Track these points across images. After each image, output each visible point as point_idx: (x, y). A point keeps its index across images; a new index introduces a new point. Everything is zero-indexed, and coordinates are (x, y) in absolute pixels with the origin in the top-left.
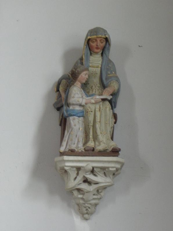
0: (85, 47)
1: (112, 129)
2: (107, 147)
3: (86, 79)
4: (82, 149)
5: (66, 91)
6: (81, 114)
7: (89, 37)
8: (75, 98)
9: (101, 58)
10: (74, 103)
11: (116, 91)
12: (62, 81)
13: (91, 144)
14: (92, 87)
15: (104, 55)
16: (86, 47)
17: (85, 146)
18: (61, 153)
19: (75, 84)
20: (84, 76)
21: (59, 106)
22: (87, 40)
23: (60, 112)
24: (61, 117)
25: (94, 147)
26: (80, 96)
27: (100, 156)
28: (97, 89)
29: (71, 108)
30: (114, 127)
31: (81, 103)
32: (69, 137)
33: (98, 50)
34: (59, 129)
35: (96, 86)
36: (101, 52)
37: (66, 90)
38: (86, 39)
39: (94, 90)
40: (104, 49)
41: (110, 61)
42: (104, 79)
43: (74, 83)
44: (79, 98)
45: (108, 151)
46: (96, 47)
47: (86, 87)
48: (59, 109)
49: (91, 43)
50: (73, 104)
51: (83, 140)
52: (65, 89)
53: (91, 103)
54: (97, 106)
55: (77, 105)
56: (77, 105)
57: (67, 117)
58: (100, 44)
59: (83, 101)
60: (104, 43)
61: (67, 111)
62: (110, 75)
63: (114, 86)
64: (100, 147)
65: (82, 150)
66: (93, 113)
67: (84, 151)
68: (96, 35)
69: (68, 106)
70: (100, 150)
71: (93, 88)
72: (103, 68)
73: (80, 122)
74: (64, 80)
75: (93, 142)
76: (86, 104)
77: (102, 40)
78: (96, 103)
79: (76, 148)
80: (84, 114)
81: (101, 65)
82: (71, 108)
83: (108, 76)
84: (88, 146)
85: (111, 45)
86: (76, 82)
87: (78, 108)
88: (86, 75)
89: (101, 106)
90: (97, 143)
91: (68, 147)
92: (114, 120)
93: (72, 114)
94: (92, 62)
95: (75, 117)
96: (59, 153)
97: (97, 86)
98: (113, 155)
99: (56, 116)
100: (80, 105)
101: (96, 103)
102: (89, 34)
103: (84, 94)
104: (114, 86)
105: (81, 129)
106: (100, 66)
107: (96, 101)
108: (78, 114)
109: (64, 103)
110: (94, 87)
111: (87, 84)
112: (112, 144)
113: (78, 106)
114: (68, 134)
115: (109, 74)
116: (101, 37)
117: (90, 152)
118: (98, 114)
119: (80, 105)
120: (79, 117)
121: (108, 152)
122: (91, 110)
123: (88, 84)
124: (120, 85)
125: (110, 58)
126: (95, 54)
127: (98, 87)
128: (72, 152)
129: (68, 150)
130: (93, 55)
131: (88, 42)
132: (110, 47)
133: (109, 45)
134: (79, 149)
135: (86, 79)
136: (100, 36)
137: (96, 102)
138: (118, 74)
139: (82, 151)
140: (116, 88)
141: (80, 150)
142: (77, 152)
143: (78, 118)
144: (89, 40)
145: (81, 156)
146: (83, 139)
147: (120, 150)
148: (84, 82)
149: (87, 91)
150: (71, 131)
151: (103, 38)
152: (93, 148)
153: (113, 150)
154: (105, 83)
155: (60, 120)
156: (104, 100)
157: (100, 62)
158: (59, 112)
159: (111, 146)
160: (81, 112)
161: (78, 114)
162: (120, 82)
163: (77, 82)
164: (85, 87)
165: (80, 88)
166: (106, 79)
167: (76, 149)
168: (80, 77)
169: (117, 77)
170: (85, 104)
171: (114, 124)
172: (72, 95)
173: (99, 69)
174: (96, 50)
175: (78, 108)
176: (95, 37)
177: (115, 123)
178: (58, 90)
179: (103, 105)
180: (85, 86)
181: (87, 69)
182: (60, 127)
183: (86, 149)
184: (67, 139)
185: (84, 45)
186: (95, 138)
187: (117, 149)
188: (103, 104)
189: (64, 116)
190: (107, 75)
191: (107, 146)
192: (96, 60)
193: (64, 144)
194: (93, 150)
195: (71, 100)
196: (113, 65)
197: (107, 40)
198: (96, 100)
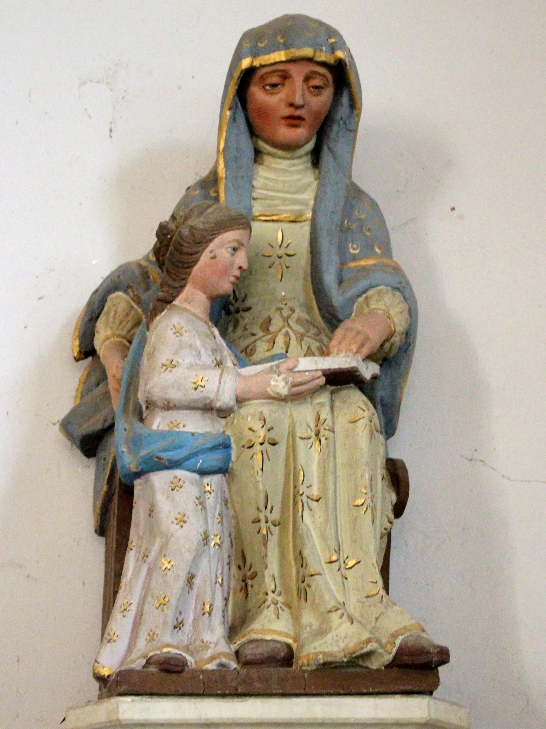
0: (228, 113)
1: (385, 539)
2: (369, 641)
3: (237, 273)
4: (226, 655)
5: (128, 349)
6: (213, 459)
7: (246, 63)
8: (177, 373)
9: (309, 178)
10: (175, 395)
11: (397, 339)
12: (108, 298)
13: (272, 626)
14: (266, 325)
15: (326, 158)
16: (234, 118)
17: (240, 641)
18: (101, 679)
19: (176, 302)
20: (224, 254)
21: (94, 425)
22: (236, 75)
23: (98, 462)
24: (105, 488)
25: (290, 641)
26: (207, 358)
27: (338, 694)
28: (296, 333)
29: (155, 427)
30: (389, 535)
31: (212, 396)
32: (147, 588)
33: (301, 132)
34: (94, 551)
35: (289, 317)
36: (310, 146)
37: (130, 342)
38: (230, 76)
39: (280, 340)
40: (323, 129)
41: (355, 194)
42: (329, 278)
43: (174, 297)
44: (204, 367)
45: (375, 664)
46: (288, 111)
47: (235, 326)
48: (91, 444)
49: (257, 93)
50: (169, 406)
51: (226, 605)
52: (119, 336)
53: (269, 397)
54: (304, 415)
55: (191, 407)
56: (191, 407)
57: (138, 475)
58: (308, 95)
59: (222, 385)
60: (328, 94)
61: (135, 442)
62: (362, 263)
63: (381, 311)
64: (337, 640)
65: (224, 660)
66: (282, 448)
67: (234, 665)
68: (286, 46)
69: (142, 420)
70: (329, 659)
71: (272, 329)
72: (321, 220)
73: (210, 500)
74: (120, 294)
75: (285, 614)
76: (240, 401)
77: (319, 74)
78: (297, 395)
79: (187, 649)
80: (228, 459)
81: (314, 211)
82: (159, 422)
83: (353, 264)
84: (254, 636)
85: (360, 109)
86: (183, 287)
87: (194, 425)
88: (235, 249)
89: (325, 414)
90: (308, 618)
91: (142, 644)
92: (393, 498)
93: (164, 455)
94: (264, 192)
95: (179, 473)
96: (96, 685)
97: (295, 315)
98: (409, 688)
99: (77, 484)
100: (208, 408)
101: (297, 395)
102: (247, 45)
103: (226, 351)
104: (381, 311)
105: (214, 541)
106: (309, 215)
107: (294, 385)
108: (194, 454)
109: (117, 403)
110: (277, 323)
111: (237, 311)
112: (391, 627)
113: (198, 415)
114: (144, 572)
115: (355, 258)
116: (310, 60)
117: (272, 670)
118: (310, 457)
119: (208, 408)
120: (203, 473)
121: (378, 670)
122: (272, 434)
123: (248, 309)
124: (412, 313)
125: (355, 179)
126: (279, 152)
127: (299, 321)
128: (163, 675)
129: (144, 662)
130: (268, 160)
131: (243, 84)
132: (358, 116)
133: (354, 105)
134: (209, 653)
135: (237, 273)
136: (308, 52)
137: (295, 390)
138: (401, 255)
139: (222, 665)
140: (400, 323)
141: (212, 658)
142: (193, 671)
143: (196, 476)
144: (250, 72)
145: (223, 696)
146: (226, 599)
147: (444, 656)
148: (225, 286)
149: (244, 344)
150: (162, 553)
151: (323, 64)
152: (289, 647)
153: (407, 659)
154: (337, 298)
155: (99, 503)
156: (338, 379)
157: (309, 196)
158: (92, 462)
159: (394, 636)
160: (214, 448)
161: (194, 454)
162: (412, 292)
163: (188, 288)
164: (231, 328)
165: (200, 319)
166: (340, 281)
167: (188, 658)
168: (204, 258)
169: (397, 270)
170: (232, 403)
171: (391, 515)
172: (163, 358)
173: (306, 228)
174: (284, 133)
175: (194, 425)
176: (280, 56)
177: (399, 509)
178: (87, 351)
179: (332, 408)
180: (228, 313)
181: (242, 221)
182: (102, 539)
183: (250, 652)
184: (135, 601)
185: (222, 107)
186: (301, 591)
187: (428, 653)
188: (332, 401)
189: (119, 474)
190: (343, 263)
191: (365, 635)
192: (284, 186)
193: (121, 625)
194: (288, 658)
195: (158, 382)
196: (374, 205)
197: (340, 76)
198: (299, 379)
